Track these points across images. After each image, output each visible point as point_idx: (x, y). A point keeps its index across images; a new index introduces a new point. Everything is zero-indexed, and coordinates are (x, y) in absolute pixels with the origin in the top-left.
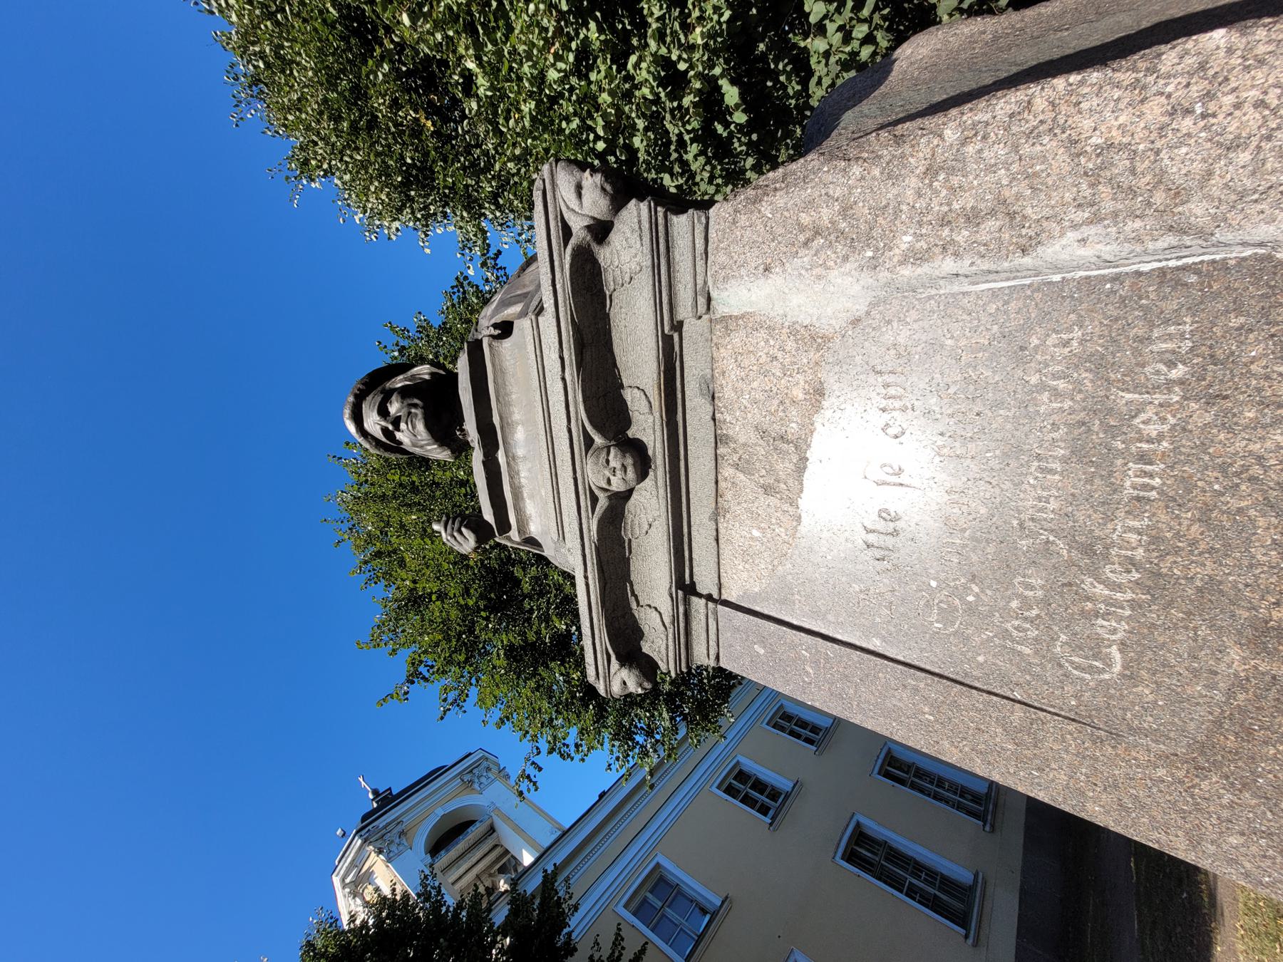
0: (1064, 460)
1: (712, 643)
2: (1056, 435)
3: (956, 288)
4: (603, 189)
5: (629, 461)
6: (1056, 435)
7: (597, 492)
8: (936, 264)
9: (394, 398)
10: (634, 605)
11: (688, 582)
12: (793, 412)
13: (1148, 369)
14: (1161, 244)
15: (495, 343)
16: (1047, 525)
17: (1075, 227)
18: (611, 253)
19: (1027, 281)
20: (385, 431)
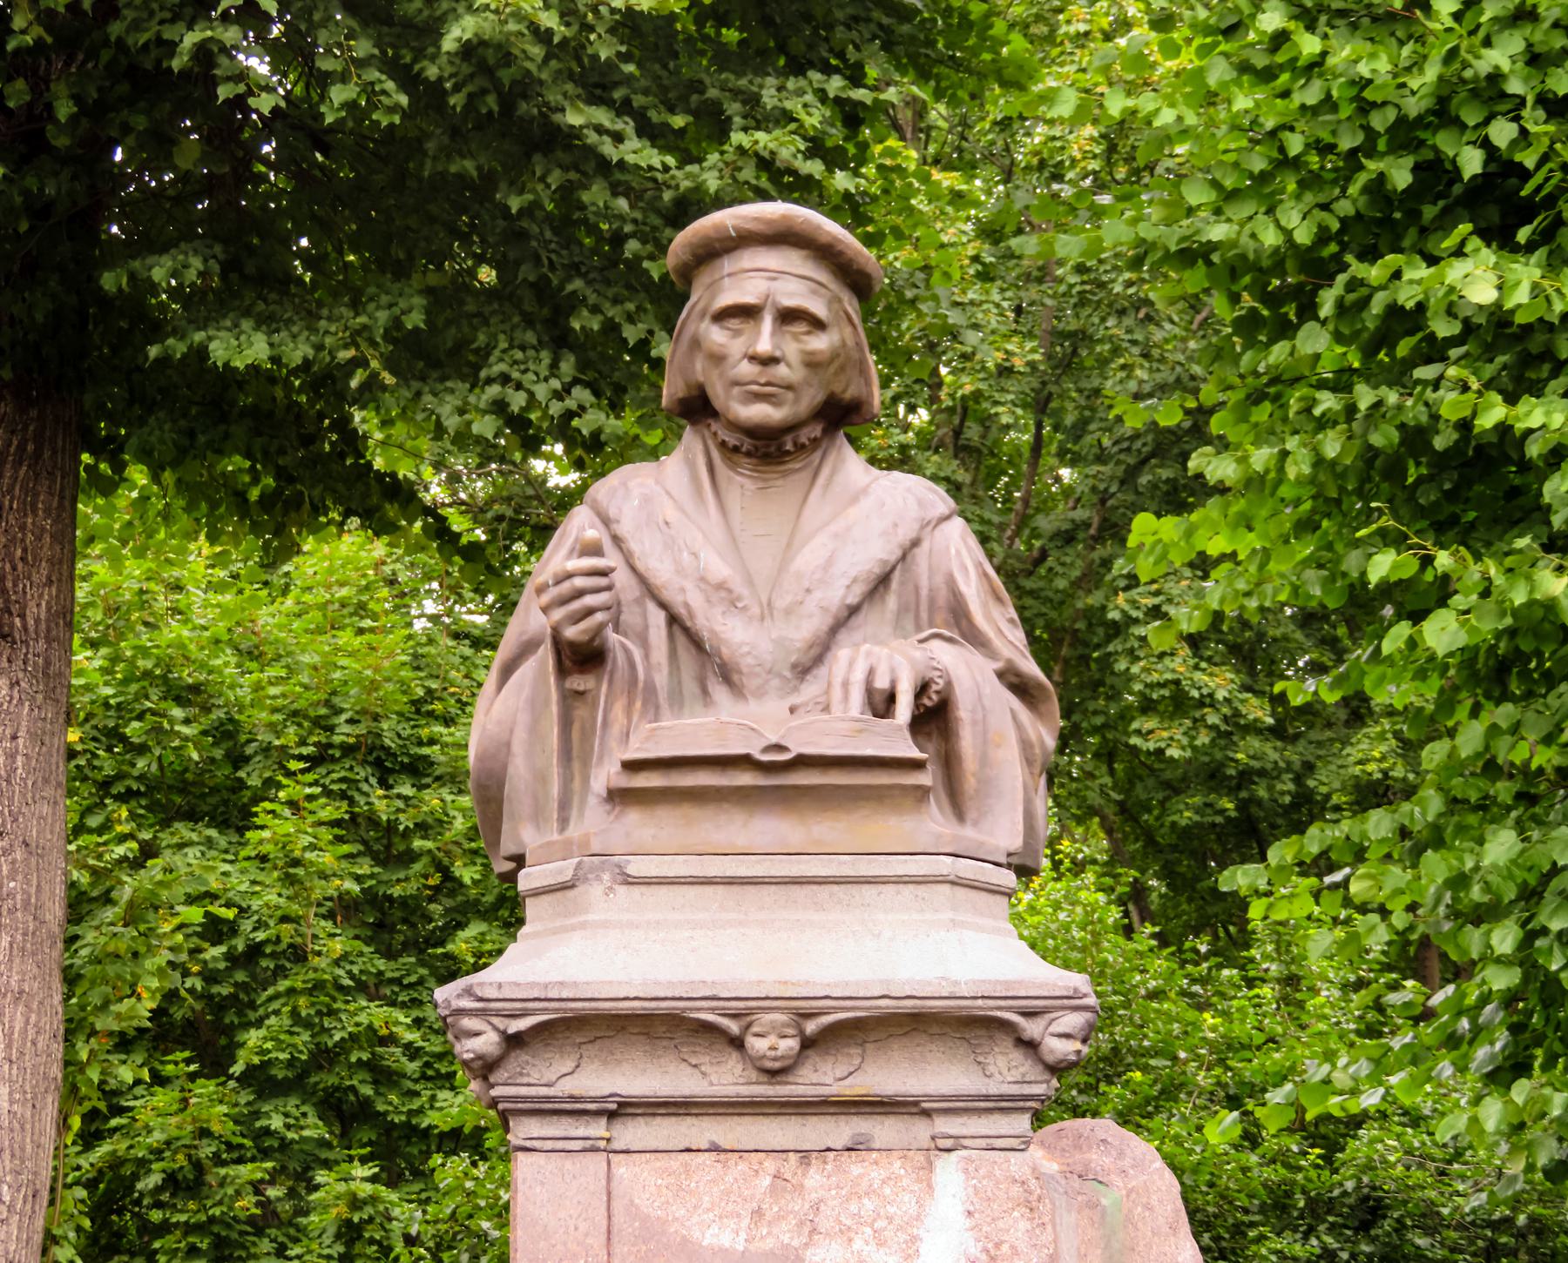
1: (549, 1145)
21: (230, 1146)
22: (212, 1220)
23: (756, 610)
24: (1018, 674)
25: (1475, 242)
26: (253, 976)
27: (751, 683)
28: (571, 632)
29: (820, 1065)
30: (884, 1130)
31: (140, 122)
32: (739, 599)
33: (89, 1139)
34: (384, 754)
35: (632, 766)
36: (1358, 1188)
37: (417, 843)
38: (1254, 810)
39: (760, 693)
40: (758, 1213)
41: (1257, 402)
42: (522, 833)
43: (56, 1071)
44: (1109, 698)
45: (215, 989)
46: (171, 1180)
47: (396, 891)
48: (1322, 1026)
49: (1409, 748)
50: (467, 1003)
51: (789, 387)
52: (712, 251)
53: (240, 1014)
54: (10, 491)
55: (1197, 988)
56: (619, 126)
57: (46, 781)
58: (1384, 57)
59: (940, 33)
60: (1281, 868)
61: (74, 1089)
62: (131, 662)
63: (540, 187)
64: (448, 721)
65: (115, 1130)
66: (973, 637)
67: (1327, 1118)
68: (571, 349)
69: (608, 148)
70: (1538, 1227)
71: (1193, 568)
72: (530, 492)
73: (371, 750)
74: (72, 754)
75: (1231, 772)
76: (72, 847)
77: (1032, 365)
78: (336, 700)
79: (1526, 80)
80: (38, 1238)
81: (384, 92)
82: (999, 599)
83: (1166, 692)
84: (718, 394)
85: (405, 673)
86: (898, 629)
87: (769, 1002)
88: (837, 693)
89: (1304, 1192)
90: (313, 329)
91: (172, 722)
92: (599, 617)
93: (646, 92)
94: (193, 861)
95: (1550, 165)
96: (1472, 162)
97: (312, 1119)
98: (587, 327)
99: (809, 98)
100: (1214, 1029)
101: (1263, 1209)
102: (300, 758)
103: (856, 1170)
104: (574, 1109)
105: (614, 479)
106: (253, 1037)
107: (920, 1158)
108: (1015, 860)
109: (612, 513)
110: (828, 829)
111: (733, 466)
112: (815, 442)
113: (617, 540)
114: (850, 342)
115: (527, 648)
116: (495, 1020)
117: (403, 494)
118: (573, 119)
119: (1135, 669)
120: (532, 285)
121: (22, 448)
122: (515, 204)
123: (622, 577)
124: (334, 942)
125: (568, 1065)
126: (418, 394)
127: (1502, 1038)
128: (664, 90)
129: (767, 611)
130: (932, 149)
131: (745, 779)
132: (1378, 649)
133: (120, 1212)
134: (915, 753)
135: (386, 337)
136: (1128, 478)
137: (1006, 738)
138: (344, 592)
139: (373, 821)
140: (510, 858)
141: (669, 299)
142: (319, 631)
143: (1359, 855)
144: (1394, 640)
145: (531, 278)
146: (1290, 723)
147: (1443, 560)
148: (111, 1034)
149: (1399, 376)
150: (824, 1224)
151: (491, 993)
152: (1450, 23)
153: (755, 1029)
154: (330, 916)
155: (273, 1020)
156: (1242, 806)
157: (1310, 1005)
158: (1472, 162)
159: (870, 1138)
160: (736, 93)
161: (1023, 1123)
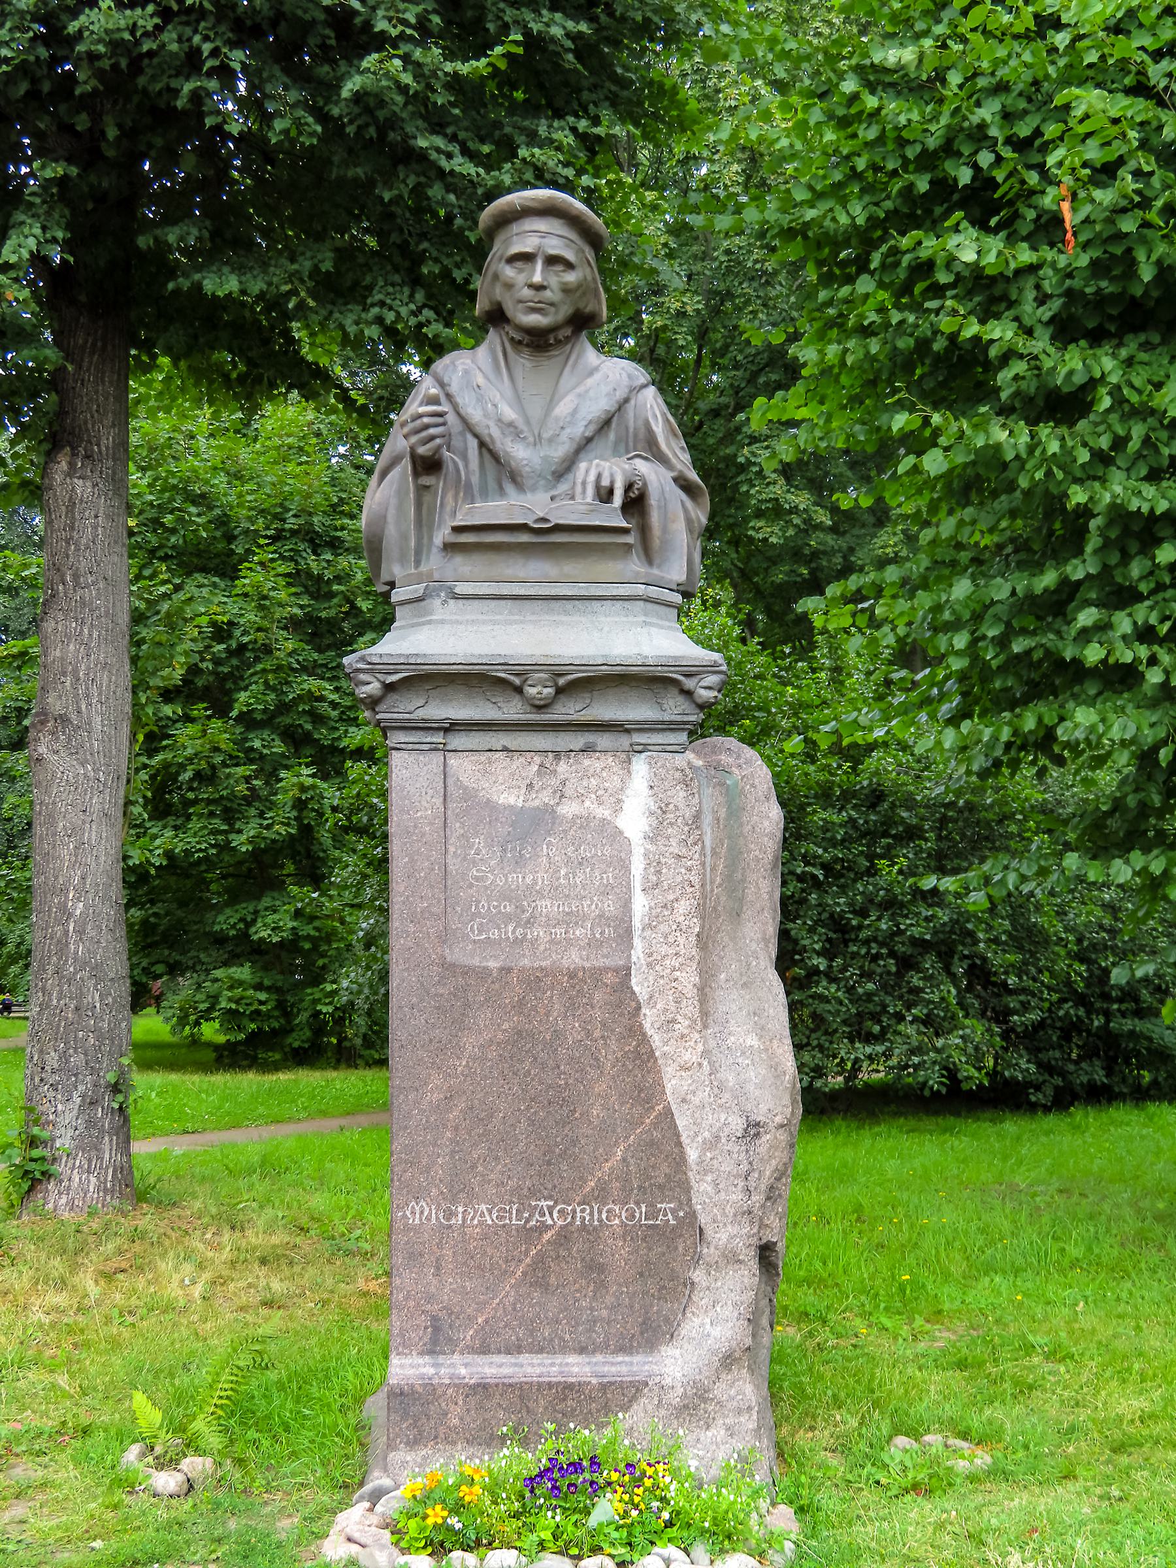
21: (231, 757)
22: (222, 797)
23: (531, 439)
24: (686, 480)
25: (965, 224)
26: (242, 662)
27: (528, 483)
28: (421, 450)
29: (568, 705)
30: (603, 740)
31: (159, 142)
32: (522, 432)
33: (151, 752)
34: (316, 535)
35: (457, 530)
36: (870, 784)
37: (335, 587)
38: (819, 574)
39: (534, 489)
40: (530, 786)
41: (831, 328)
42: (394, 569)
43: (128, 709)
44: (737, 509)
45: (221, 669)
46: (198, 775)
47: (323, 615)
48: (853, 695)
49: (910, 539)
50: (361, 666)
51: (552, 304)
52: (506, 219)
53: (235, 683)
54: (88, 370)
55: (783, 673)
56: (450, 148)
57: (116, 542)
58: (916, 111)
59: (647, 97)
60: (833, 599)
61: (139, 718)
62: (166, 479)
63: (402, 186)
64: (353, 517)
65: (165, 747)
66: (661, 459)
67: (854, 745)
68: (422, 286)
69: (444, 163)
70: (970, 807)
71: (792, 423)
72: (399, 382)
73: (307, 533)
74: (131, 534)
75: (807, 552)
76: (134, 588)
77: (698, 311)
78: (287, 503)
79: (1001, 128)
80: (121, 802)
81: (307, 124)
82: (675, 435)
83: (770, 505)
84: (510, 309)
85: (328, 489)
86: (616, 453)
87: (537, 667)
88: (579, 489)
89: (840, 786)
90: (265, 272)
91: (190, 514)
92: (438, 441)
93: (466, 130)
94: (207, 601)
95: (1012, 180)
96: (965, 176)
97: (277, 742)
98: (433, 277)
99: (567, 132)
100: (792, 696)
101: (816, 796)
102: (266, 537)
103: (587, 762)
104: (425, 727)
105: (447, 360)
106: (243, 696)
107: (623, 756)
108: (681, 588)
109: (446, 380)
110: (572, 568)
111: (518, 352)
112: (568, 338)
113: (449, 396)
114: (589, 278)
115: (395, 461)
117: (322, 375)
118: (422, 143)
119: (752, 492)
120: (399, 246)
121: (94, 345)
122: (387, 196)
123: (451, 418)
124: (286, 643)
125: (421, 702)
126: (331, 313)
127: (956, 700)
128: (479, 128)
129: (538, 441)
130: (640, 177)
131: (524, 538)
132: (895, 472)
133: (170, 793)
134: (624, 524)
135: (310, 277)
136: (752, 379)
137: (678, 518)
138: (290, 440)
139: (309, 574)
140: (386, 584)
141: (479, 254)
142: (275, 463)
143: (879, 592)
144: (908, 462)
145: (398, 241)
146: (845, 520)
147: (936, 419)
148: (159, 688)
149: (917, 308)
150: (568, 792)
151: (376, 660)
152: (956, 90)
154: (285, 628)
155: (254, 687)
156: (812, 572)
157: (847, 683)
158: (965, 176)
159: (595, 744)
160: (522, 130)
161: (683, 737)
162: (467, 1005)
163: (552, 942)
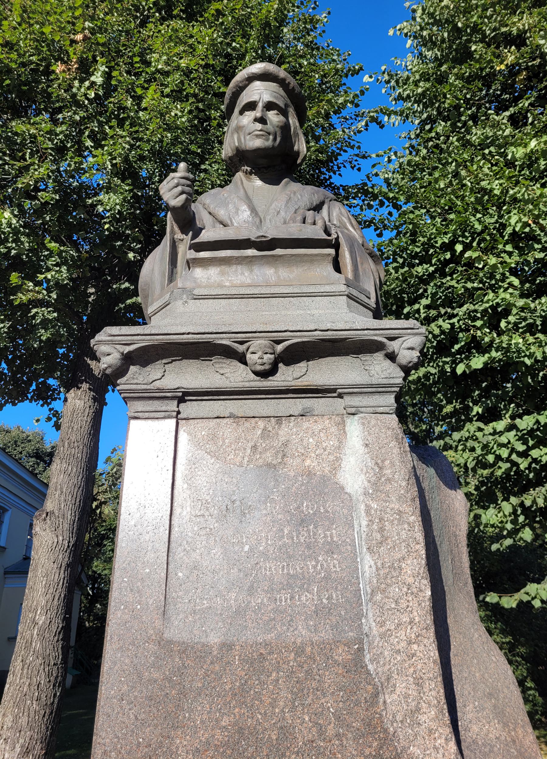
0: (288, 574)
2: (298, 569)
3: (356, 526)
4: (410, 362)
5: (267, 367)
6: (298, 569)
7: (247, 344)
8: (365, 519)
9: (282, 118)
10: (164, 361)
11: (186, 398)
12: (299, 460)
13: (326, 593)
14: (368, 589)
15: (330, 258)
16: (259, 573)
17: (375, 564)
18: (380, 360)
19: (358, 551)
20: (251, 106)
103: (306, 425)
104: (160, 396)
107: (338, 419)
116: (118, 347)
153: (251, 350)
162: (183, 693)
163: (276, 611)
